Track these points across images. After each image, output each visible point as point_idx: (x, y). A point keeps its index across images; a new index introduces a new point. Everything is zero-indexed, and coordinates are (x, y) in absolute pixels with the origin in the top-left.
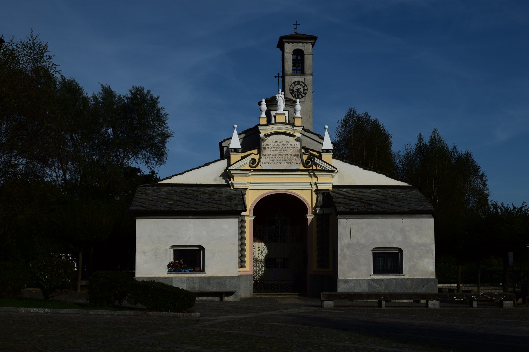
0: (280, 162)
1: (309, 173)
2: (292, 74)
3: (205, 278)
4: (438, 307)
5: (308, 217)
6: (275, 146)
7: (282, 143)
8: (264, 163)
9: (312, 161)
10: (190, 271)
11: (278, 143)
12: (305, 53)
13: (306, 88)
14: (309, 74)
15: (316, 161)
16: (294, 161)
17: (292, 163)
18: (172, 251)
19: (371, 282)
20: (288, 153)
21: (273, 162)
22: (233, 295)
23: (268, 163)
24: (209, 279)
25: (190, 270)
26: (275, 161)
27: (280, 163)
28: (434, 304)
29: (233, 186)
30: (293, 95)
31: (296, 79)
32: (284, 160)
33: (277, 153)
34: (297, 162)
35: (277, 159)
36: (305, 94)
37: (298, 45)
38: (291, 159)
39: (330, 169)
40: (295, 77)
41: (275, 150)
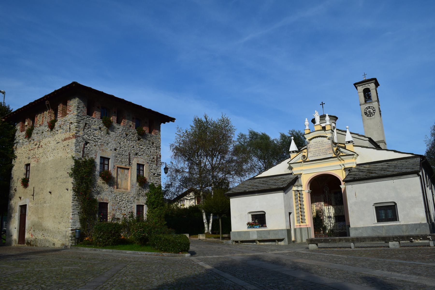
0: (320, 154)
1: (338, 158)
2: (364, 103)
3: (267, 230)
4: (397, 247)
5: (341, 187)
7: (320, 143)
9: (339, 150)
10: (259, 227)
11: (317, 143)
12: (370, 90)
13: (374, 109)
14: (375, 101)
15: (341, 150)
16: (328, 153)
17: (327, 154)
18: (250, 216)
19: (373, 228)
20: (324, 148)
21: (315, 155)
22: (283, 241)
23: (312, 157)
24: (269, 232)
25: (259, 226)
26: (316, 154)
28: (394, 245)
29: (294, 174)
30: (367, 115)
31: (367, 105)
32: (322, 153)
33: (317, 149)
35: (318, 153)
36: (374, 113)
37: (365, 86)
38: (326, 151)
39: (351, 154)
40: (367, 104)
41: (316, 148)
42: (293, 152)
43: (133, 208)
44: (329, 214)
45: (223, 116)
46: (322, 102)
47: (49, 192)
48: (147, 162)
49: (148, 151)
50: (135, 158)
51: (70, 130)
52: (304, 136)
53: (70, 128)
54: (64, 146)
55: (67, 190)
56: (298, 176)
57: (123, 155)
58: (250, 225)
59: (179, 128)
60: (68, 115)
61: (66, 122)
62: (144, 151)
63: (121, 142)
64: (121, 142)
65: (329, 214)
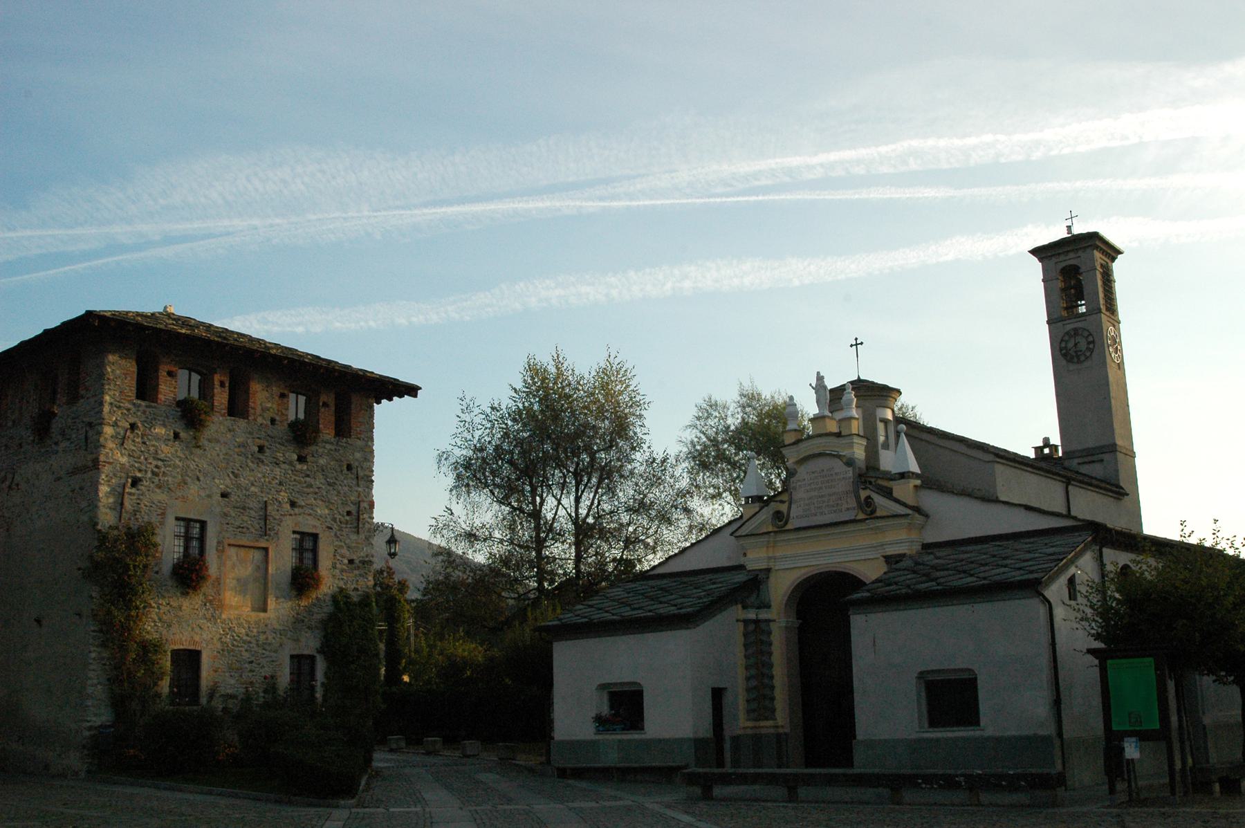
6: (811, 481)
13: (1091, 339)
16: (845, 506)
23: (802, 517)
24: (648, 744)
27: (821, 513)
34: (850, 506)
36: (1092, 351)
37: (1068, 258)
39: (903, 513)
45: (612, 357)
46: (856, 339)
47: (35, 620)
51: (87, 446)
52: (781, 452)
53: (86, 438)
54: (72, 491)
55: (78, 617)
56: (758, 575)
58: (602, 722)
59: (468, 401)
60: (82, 401)
61: (77, 420)
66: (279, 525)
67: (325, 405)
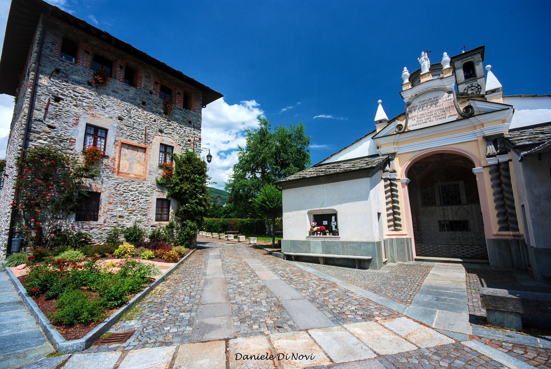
0: (430, 120)
8: (411, 126)
11: (426, 102)
24: (346, 244)
35: (426, 117)
42: (381, 121)
43: (150, 203)
44: (444, 217)
48: (179, 143)
49: (180, 129)
50: (157, 135)
57: (134, 128)
62: (173, 129)
63: (131, 110)
64: (131, 110)
65: (444, 217)
66: (153, 139)
67: (179, 93)
